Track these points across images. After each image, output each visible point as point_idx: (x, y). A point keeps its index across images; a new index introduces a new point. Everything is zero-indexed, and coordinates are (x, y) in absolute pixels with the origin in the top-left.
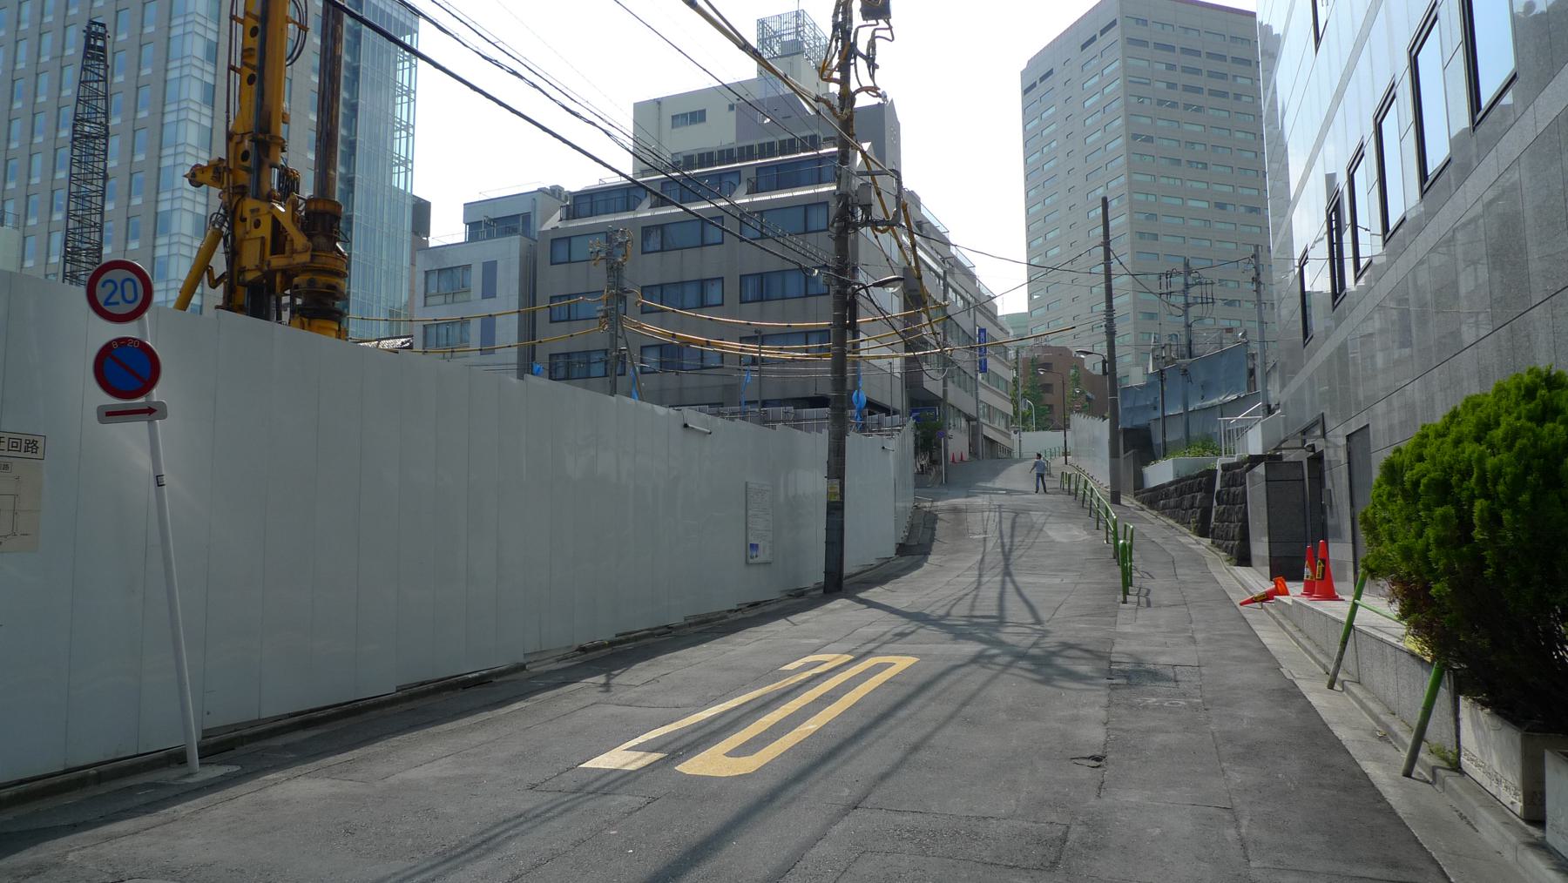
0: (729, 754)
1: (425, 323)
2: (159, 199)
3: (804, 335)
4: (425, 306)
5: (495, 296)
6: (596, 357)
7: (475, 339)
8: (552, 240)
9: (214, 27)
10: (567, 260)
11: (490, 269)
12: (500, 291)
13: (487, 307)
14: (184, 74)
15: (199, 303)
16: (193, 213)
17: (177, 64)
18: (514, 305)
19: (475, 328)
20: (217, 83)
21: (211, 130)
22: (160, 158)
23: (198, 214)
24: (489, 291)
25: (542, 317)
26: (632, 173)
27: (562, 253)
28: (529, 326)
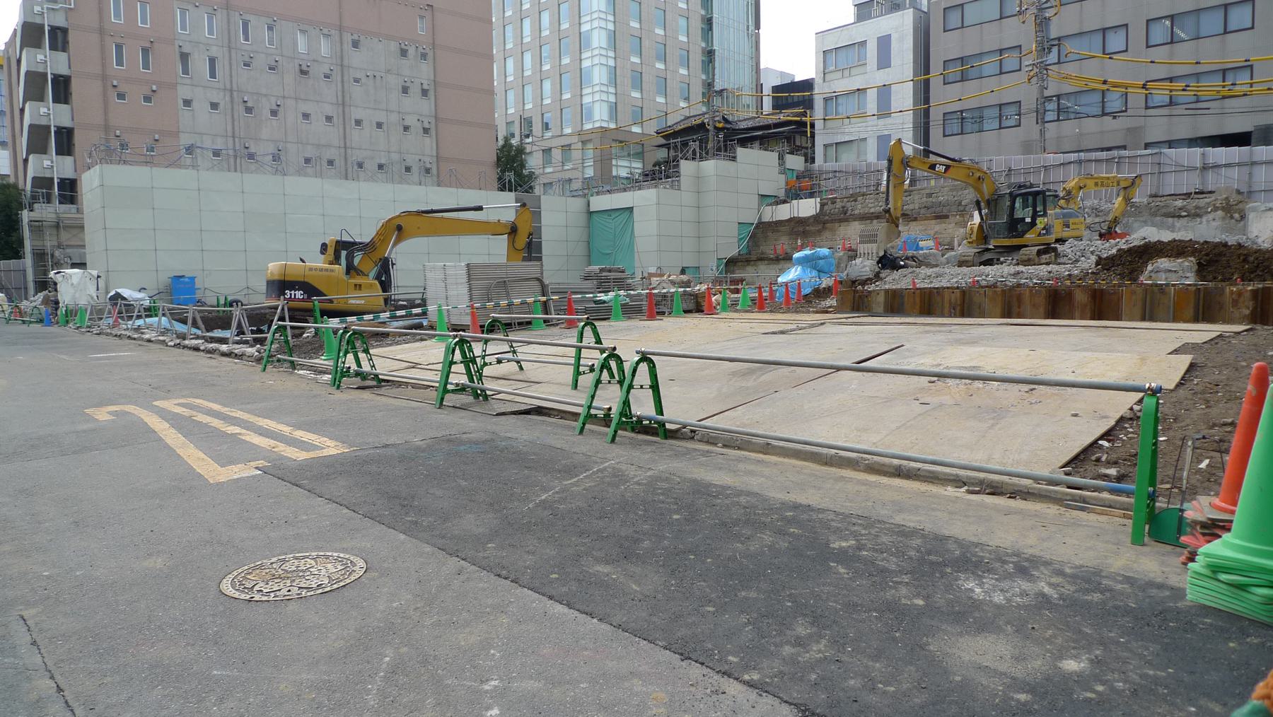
0: (108, 413)
1: (825, 96)
2: (583, 94)
3: (1221, 72)
4: (739, 223)
5: (890, 67)
6: (986, 113)
7: (871, 105)
8: (945, 9)
9: (611, 54)
10: (960, 26)
11: (884, 43)
12: (895, 61)
13: (882, 77)
14: (594, 63)
15: (614, 65)
16: (607, 66)
17: (588, 18)
18: (908, 71)
19: (872, 96)
20: (618, 101)
21: (615, 31)
22: (581, 60)
23: (609, 30)
24: (884, 61)
25: (936, 83)
26: (812, 201)
27: (954, 19)
28: (923, 92)
